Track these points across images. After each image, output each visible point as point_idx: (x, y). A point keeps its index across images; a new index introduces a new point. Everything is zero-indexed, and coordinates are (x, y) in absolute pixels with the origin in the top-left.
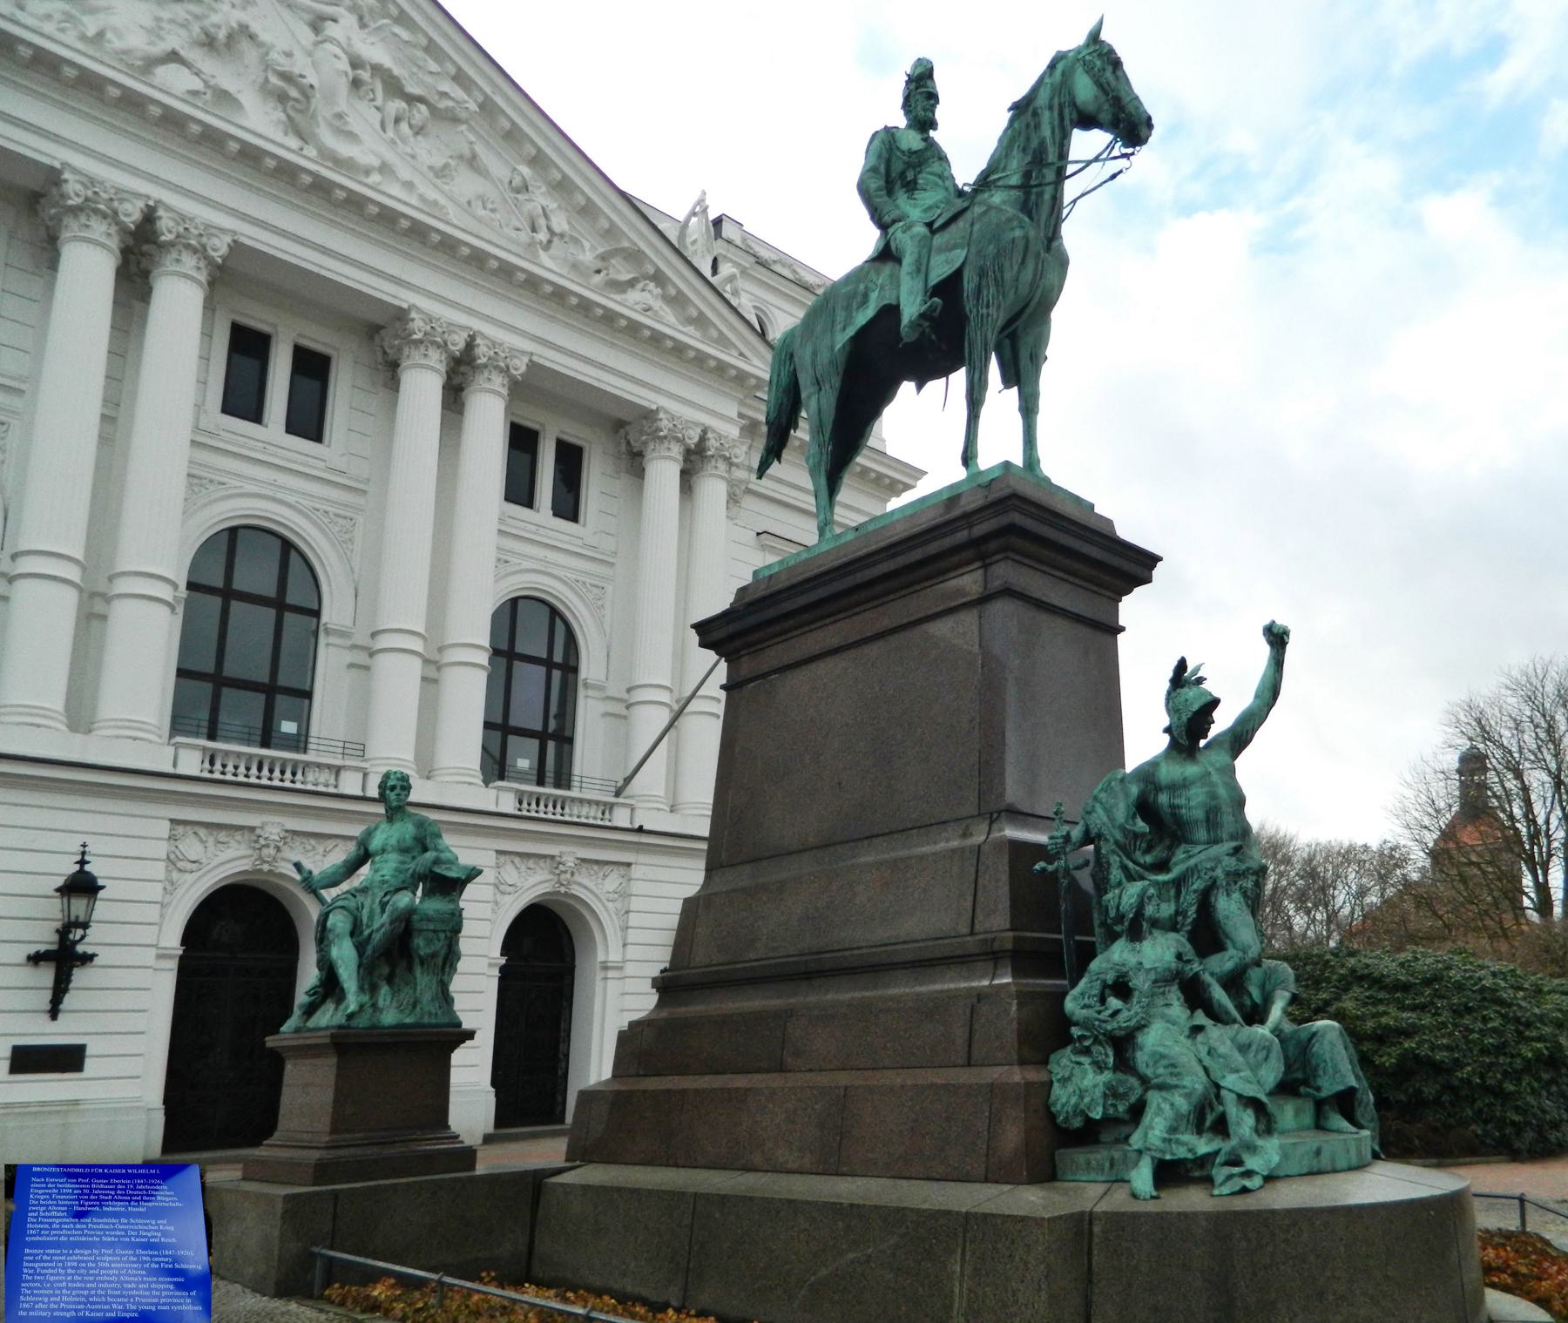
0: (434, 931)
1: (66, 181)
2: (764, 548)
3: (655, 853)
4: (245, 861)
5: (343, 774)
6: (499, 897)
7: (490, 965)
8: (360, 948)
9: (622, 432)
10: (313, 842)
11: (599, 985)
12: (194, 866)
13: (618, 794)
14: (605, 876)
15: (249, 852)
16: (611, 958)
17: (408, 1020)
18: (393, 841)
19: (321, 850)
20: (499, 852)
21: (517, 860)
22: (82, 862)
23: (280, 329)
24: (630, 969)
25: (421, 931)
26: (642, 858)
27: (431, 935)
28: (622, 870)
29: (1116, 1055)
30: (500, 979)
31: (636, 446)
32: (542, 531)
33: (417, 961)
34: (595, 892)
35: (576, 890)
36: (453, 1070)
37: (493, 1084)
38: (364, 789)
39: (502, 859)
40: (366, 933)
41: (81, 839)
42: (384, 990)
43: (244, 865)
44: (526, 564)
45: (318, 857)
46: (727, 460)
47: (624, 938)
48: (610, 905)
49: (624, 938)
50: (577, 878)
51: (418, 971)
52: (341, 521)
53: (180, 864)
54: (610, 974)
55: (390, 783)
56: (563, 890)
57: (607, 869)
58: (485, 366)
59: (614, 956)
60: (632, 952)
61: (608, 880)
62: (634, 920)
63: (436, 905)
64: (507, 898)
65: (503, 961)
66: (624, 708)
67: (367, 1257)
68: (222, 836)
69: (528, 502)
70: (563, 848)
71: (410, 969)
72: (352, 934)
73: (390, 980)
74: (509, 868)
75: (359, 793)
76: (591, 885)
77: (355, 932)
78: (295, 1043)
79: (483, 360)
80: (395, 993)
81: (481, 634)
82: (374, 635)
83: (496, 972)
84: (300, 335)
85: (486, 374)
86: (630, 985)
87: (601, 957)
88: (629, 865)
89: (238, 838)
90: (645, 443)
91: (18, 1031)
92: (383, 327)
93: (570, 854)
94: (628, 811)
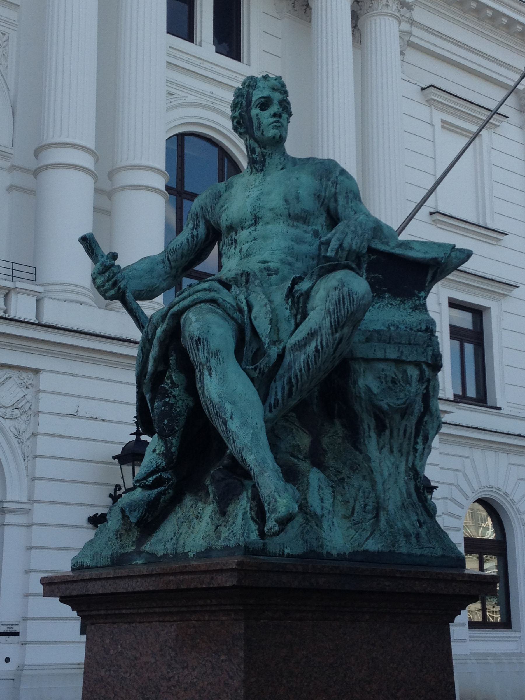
0: (398, 362)
2: (429, 102)
5: (13, 297)
8: (263, 382)
16: (9, 498)
17: (373, 545)
18: (275, 200)
24: (40, 513)
25: (367, 360)
27: (391, 370)
29: (184, 589)
32: (206, 65)
33: (368, 423)
36: (452, 644)
38: (37, 316)
40: (274, 351)
42: (315, 477)
44: (192, 98)
51: (372, 446)
55: (257, 95)
63: (385, 315)
69: (189, 35)
71: (354, 437)
72: (239, 354)
73: (317, 458)
75: (36, 321)
77: (247, 344)
78: (109, 588)
80: (338, 483)
81: (158, 158)
82: (37, 152)
88: (37, 371)
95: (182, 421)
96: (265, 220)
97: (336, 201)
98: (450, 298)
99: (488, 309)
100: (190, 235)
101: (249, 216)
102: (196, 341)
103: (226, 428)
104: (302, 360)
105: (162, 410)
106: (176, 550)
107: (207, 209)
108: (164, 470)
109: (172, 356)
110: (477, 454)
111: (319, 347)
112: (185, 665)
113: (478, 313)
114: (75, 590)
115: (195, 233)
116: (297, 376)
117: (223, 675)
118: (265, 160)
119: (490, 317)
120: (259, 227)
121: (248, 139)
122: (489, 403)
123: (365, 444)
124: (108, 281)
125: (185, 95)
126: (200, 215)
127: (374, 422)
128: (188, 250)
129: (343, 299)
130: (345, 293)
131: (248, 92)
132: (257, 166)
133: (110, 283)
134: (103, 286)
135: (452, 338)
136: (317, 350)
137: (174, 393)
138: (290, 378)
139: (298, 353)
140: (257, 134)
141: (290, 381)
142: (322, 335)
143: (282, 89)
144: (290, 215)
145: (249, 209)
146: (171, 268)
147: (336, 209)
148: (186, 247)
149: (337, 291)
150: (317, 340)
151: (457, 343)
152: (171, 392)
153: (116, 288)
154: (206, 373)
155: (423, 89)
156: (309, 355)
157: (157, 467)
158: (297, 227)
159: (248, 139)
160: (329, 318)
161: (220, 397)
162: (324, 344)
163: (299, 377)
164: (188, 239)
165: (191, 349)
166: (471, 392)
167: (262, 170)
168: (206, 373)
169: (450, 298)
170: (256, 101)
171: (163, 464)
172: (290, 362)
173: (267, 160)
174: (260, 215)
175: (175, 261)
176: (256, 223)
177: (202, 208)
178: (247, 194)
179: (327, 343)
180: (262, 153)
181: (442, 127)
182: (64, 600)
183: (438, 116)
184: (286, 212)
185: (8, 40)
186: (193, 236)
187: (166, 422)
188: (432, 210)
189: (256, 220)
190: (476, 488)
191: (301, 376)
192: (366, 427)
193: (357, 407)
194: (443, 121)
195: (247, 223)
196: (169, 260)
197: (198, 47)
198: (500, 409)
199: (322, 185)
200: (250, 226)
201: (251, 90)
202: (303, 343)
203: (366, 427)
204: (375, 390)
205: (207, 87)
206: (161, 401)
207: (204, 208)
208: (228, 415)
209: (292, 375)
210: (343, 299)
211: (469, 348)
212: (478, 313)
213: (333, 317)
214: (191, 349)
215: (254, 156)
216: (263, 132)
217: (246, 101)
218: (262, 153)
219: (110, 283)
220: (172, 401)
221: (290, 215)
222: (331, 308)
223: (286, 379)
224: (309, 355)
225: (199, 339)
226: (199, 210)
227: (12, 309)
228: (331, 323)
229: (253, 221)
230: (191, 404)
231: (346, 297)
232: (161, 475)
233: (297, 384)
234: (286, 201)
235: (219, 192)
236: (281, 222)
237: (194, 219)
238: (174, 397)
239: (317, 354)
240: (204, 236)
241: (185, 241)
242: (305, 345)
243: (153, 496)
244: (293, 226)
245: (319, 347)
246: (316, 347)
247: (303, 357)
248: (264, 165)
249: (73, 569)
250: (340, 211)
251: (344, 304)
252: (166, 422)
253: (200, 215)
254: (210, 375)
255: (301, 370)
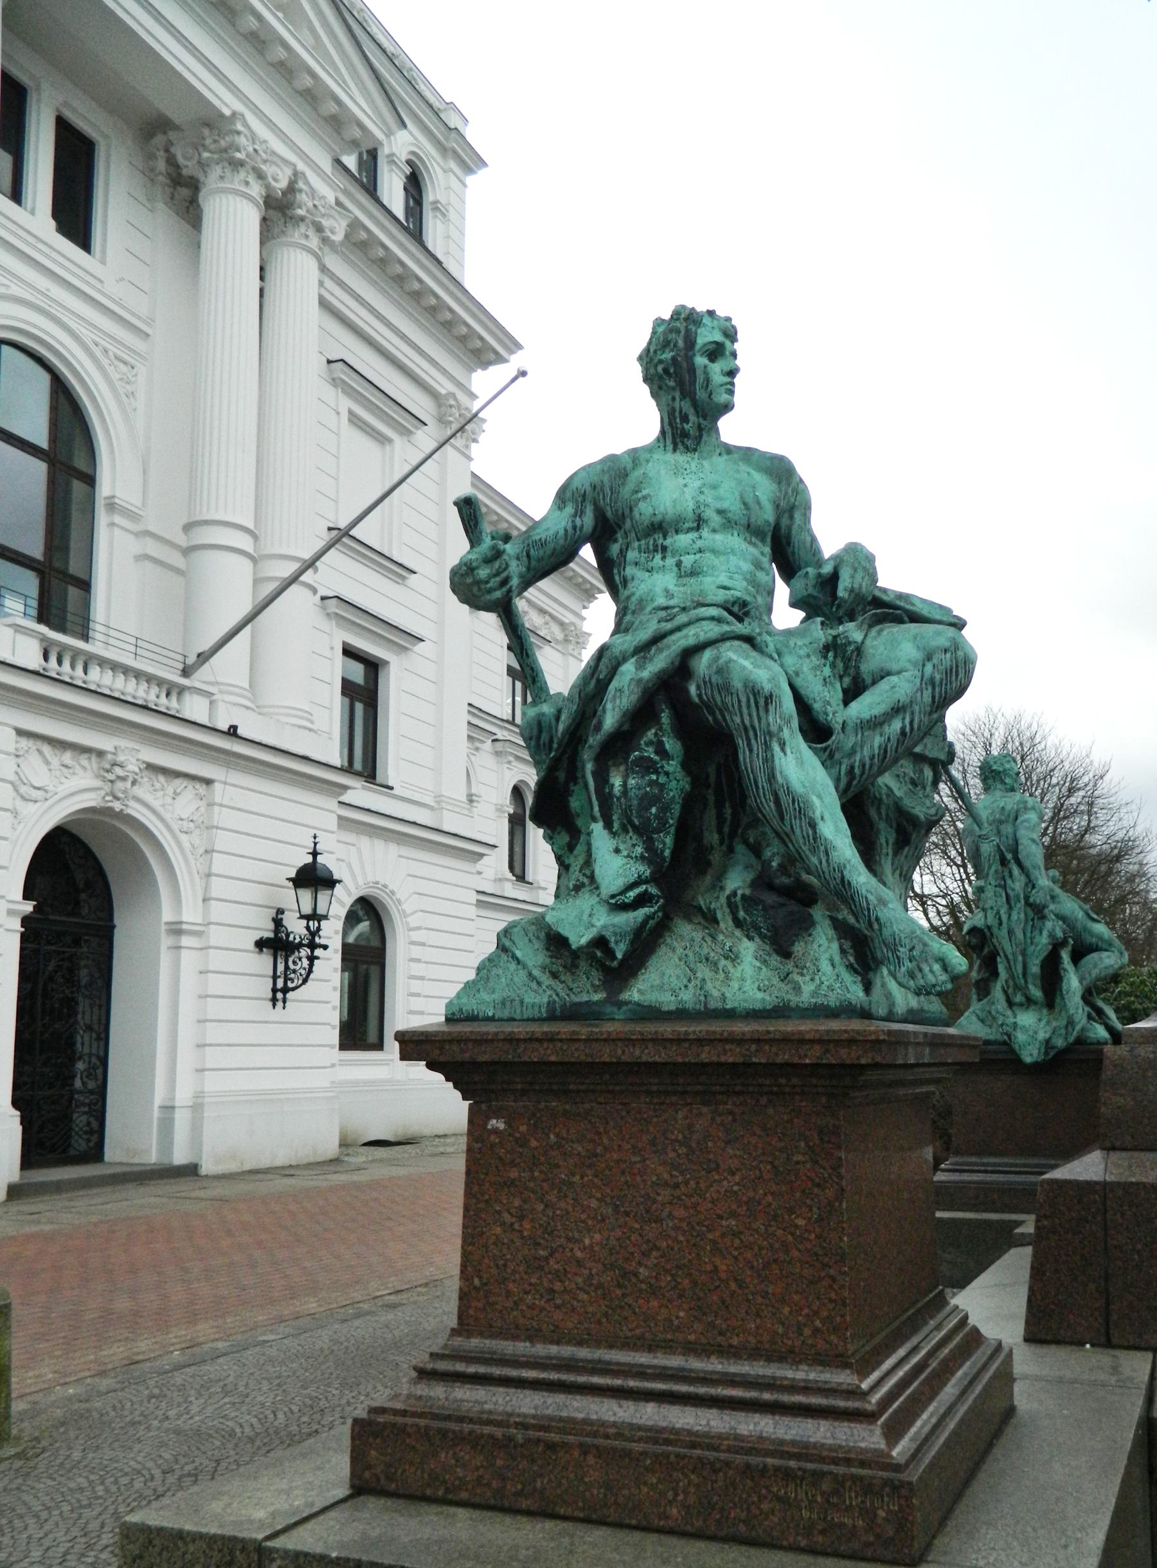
1: (300, 191)
2: (335, 382)
3: (320, 791)
4: (92, 795)
6: (19, 803)
7: (11, 913)
9: (159, 140)
10: (162, 778)
11: (165, 959)
12: (38, 794)
13: (186, 672)
14: (176, 794)
15: (98, 783)
19: (170, 791)
20: (21, 733)
21: (46, 749)
22: (315, 854)
23: (45, 85)
24: (217, 936)
26: (235, 777)
28: (202, 789)
30: (24, 938)
31: (189, 167)
34: (164, 811)
35: (135, 810)
37: (16, 1103)
39: (25, 743)
41: (312, 832)
43: (90, 800)
44: (16, 290)
45: (169, 800)
46: (319, 229)
47: (207, 888)
48: (184, 838)
49: (207, 888)
50: (138, 791)
52: (122, 366)
53: (23, 789)
54: (186, 941)
56: (117, 806)
57: (179, 783)
58: (302, 219)
59: (191, 914)
60: (218, 911)
61: (181, 800)
62: (219, 864)
64: (31, 808)
65: (28, 907)
66: (185, 549)
67: (953, 1220)
68: (68, 757)
70: (122, 743)
74: (35, 759)
76: (156, 804)
79: (301, 212)
83: (16, 925)
84: (66, 104)
85: (303, 229)
86: (217, 960)
87: (167, 915)
88: (208, 782)
89: (85, 763)
90: (203, 165)
91: (239, 1018)
92: (177, 128)
93: (134, 754)
94: (206, 702)
95: (676, 809)
96: (712, 524)
97: (791, 517)
98: (344, 643)
99: (386, 663)
100: (570, 524)
101: (691, 515)
102: (766, 698)
103: (815, 832)
104: (876, 745)
105: (647, 793)
106: (705, 1003)
107: (602, 490)
108: (646, 882)
109: (663, 711)
110: (365, 842)
111: (908, 729)
112: (713, 1166)
113: (373, 666)
114: (456, 1053)
115: (578, 521)
116: (864, 766)
117: (799, 1182)
118: (701, 436)
119: (389, 674)
120: (705, 532)
121: (678, 399)
122: (379, 780)
123: (881, 865)
124: (496, 575)
125: (7, 282)
126: (589, 497)
127: (894, 835)
128: (563, 546)
129: (957, 667)
130: (960, 659)
131: (687, 330)
132: (689, 443)
133: (498, 579)
134: (487, 582)
135: (343, 693)
136: (903, 733)
137: (667, 768)
138: (852, 768)
139: (870, 732)
140: (701, 395)
141: (851, 769)
142: (912, 713)
143: (731, 334)
144: (749, 526)
145: (691, 505)
146: (529, 569)
147: (790, 528)
148: (561, 542)
149: (948, 655)
150: (904, 719)
151: (347, 700)
152: (662, 767)
153: (504, 589)
154: (776, 748)
155: (329, 362)
156: (889, 739)
157: (639, 876)
158: (754, 545)
159: (678, 399)
160: (930, 690)
161: (804, 786)
162: (916, 726)
163: (867, 766)
164: (566, 530)
165: (749, 706)
166: (358, 766)
167: (695, 450)
168: (776, 748)
169: (344, 643)
170: (705, 345)
171: (648, 873)
172: (856, 743)
173: (705, 437)
174: (705, 516)
175: (539, 560)
176: (698, 528)
177: (595, 487)
178: (681, 481)
179: (919, 726)
180: (699, 425)
181: (349, 420)
182: (431, 1066)
183: (346, 404)
184: (744, 521)
185: (136, 375)
186: (574, 527)
187: (654, 810)
188: (332, 525)
189: (699, 522)
190: (361, 882)
191: (871, 766)
192: (883, 841)
193: (873, 813)
194: (350, 412)
195: (687, 525)
196: (528, 556)
197: (27, 214)
198: (391, 788)
199: (780, 491)
200: (689, 530)
201: (692, 327)
202: (882, 719)
203: (883, 841)
204: (898, 793)
205: (42, 282)
206: (643, 777)
207: (598, 488)
208: (818, 814)
209: (857, 764)
210: (957, 667)
211: (359, 707)
212: (373, 666)
213: (937, 689)
214: (749, 706)
215: (686, 426)
216: (711, 394)
217: (685, 342)
218: (699, 425)
219: (498, 579)
220: (662, 779)
221: (749, 526)
222: (938, 677)
223: (844, 768)
224: (889, 739)
225: (771, 695)
226: (589, 489)
227: (99, 580)
228: (933, 697)
229: (695, 525)
230: (687, 787)
231: (961, 665)
232: (646, 890)
233: (861, 776)
234: (745, 504)
235: (625, 469)
236: (736, 534)
237: (577, 501)
238: (667, 774)
239: (901, 739)
240: (590, 530)
241: (562, 532)
242: (881, 724)
243: (640, 920)
244: (750, 543)
245: (908, 729)
246: (903, 729)
247: (877, 741)
248: (699, 443)
249: (449, 1020)
250: (794, 532)
251: (957, 675)
252: (654, 810)
253: (589, 497)
254: (783, 750)
255: (872, 758)
